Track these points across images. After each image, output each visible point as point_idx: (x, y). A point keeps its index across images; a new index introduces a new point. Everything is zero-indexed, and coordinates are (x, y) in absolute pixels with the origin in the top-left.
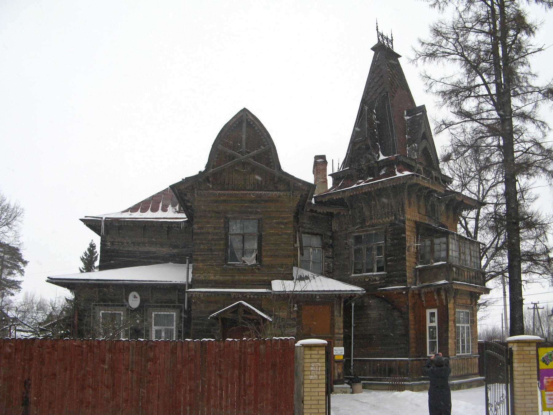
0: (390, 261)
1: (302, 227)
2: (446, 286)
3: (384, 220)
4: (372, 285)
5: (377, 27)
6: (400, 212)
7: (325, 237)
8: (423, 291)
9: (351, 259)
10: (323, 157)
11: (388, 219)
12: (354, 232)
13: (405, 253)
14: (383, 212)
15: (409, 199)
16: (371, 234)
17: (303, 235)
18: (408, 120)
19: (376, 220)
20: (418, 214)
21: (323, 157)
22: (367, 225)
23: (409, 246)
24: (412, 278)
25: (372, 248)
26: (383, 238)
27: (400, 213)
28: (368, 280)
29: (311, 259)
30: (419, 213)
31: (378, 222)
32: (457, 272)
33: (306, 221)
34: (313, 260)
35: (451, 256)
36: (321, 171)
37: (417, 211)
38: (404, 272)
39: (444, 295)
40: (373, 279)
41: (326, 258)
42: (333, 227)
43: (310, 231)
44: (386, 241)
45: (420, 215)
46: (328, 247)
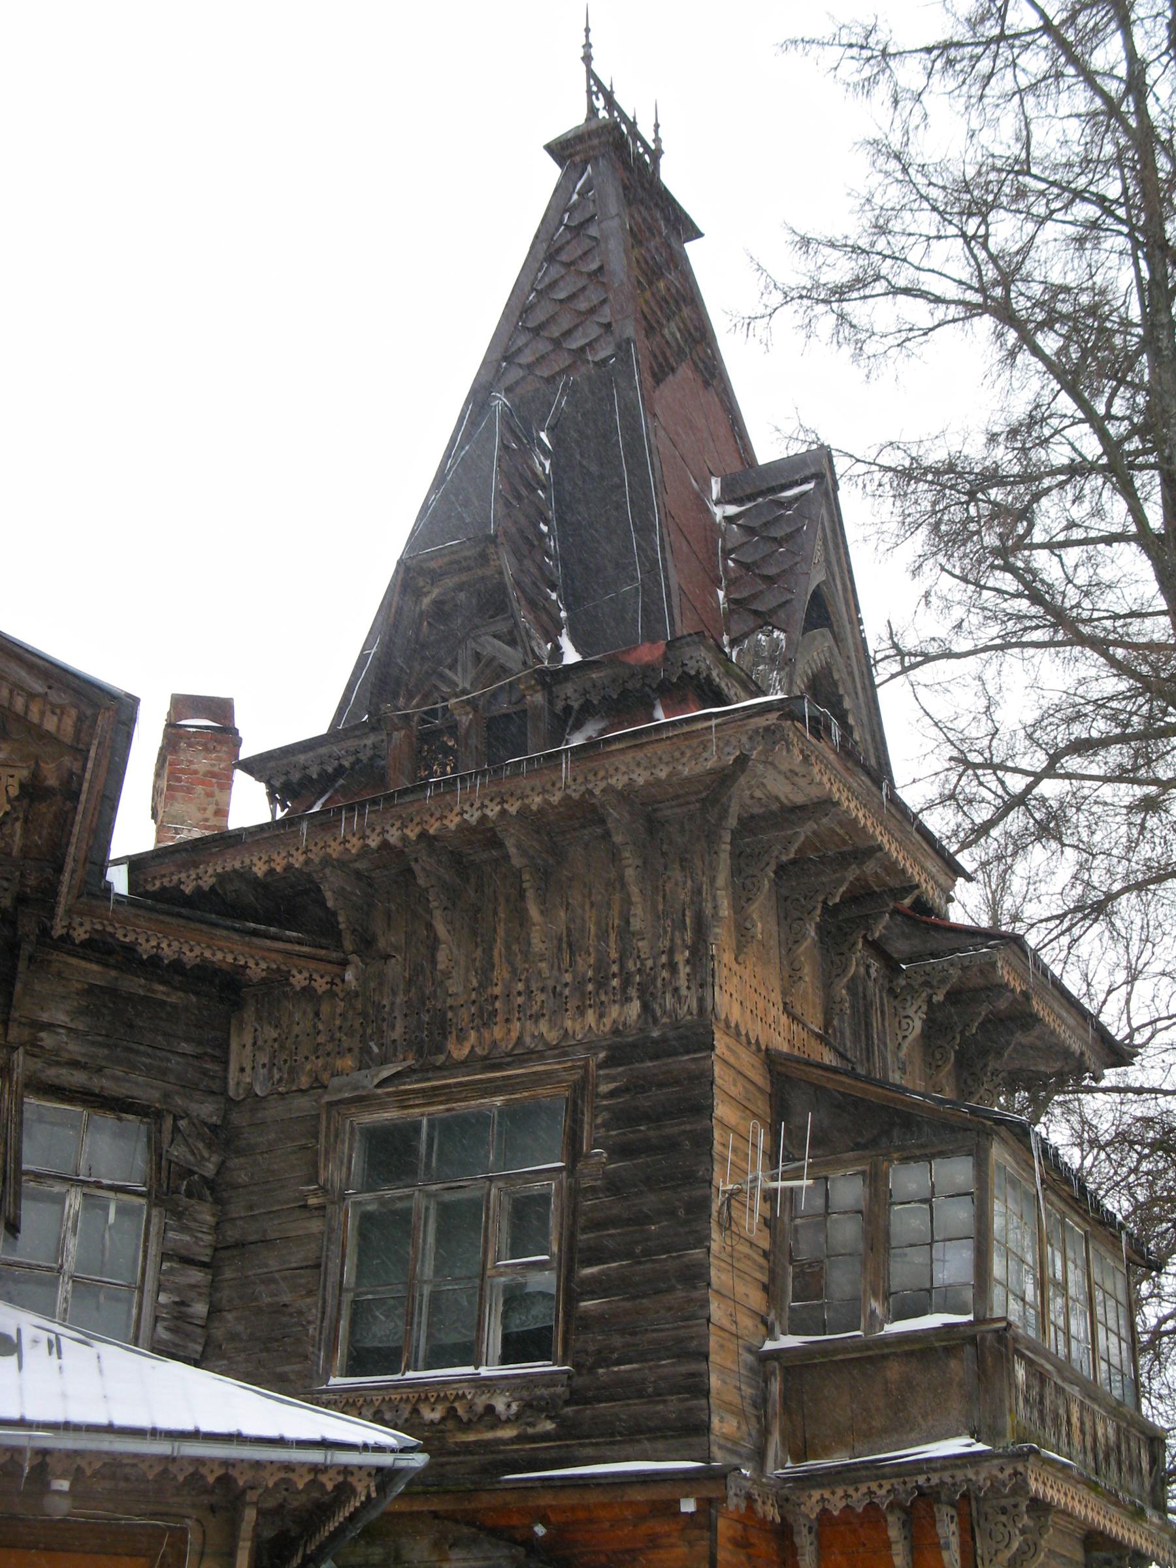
0: (595, 1288)
1: (34, 1048)
2: (981, 1476)
3: (568, 1024)
4: (467, 1448)
5: (588, 46)
6: (684, 970)
7: (176, 1129)
8: (811, 1503)
9: (332, 1279)
10: (221, 709)
11: (601, 1016)
12: (363, 1101)
13: (702, 1240)
14: (568, 978)
15: (742, 896)
16: (481, 1120)
17: (31, 1101)
18: (729, 519)
19: (516, 1026)
20: (784, 1019)
21: (221, 709)
22: (455, 1055)
23: (732, 1194)
24: (741, 1414)
25: (477, 1206)
26: (557, 1137)
27: (682, 982)
28: (436, 1416)
29: (69, 1265)
30: (793, 1017)
31: (528, 1040)
32: (1034, 1392)
33: (62, 1018)
34: (79, 1264)
35: (997, 1281)
36: (203, 783)
37: (776, 997)
38: (693, 1367)
39: (954, 1541)
40: (470, 1407)
41: (166, 1265)
42: (233, 1067)
43: (78, 1078)
44: (574, 1154)
45: (794, 1027)
46: (189, 1194)
